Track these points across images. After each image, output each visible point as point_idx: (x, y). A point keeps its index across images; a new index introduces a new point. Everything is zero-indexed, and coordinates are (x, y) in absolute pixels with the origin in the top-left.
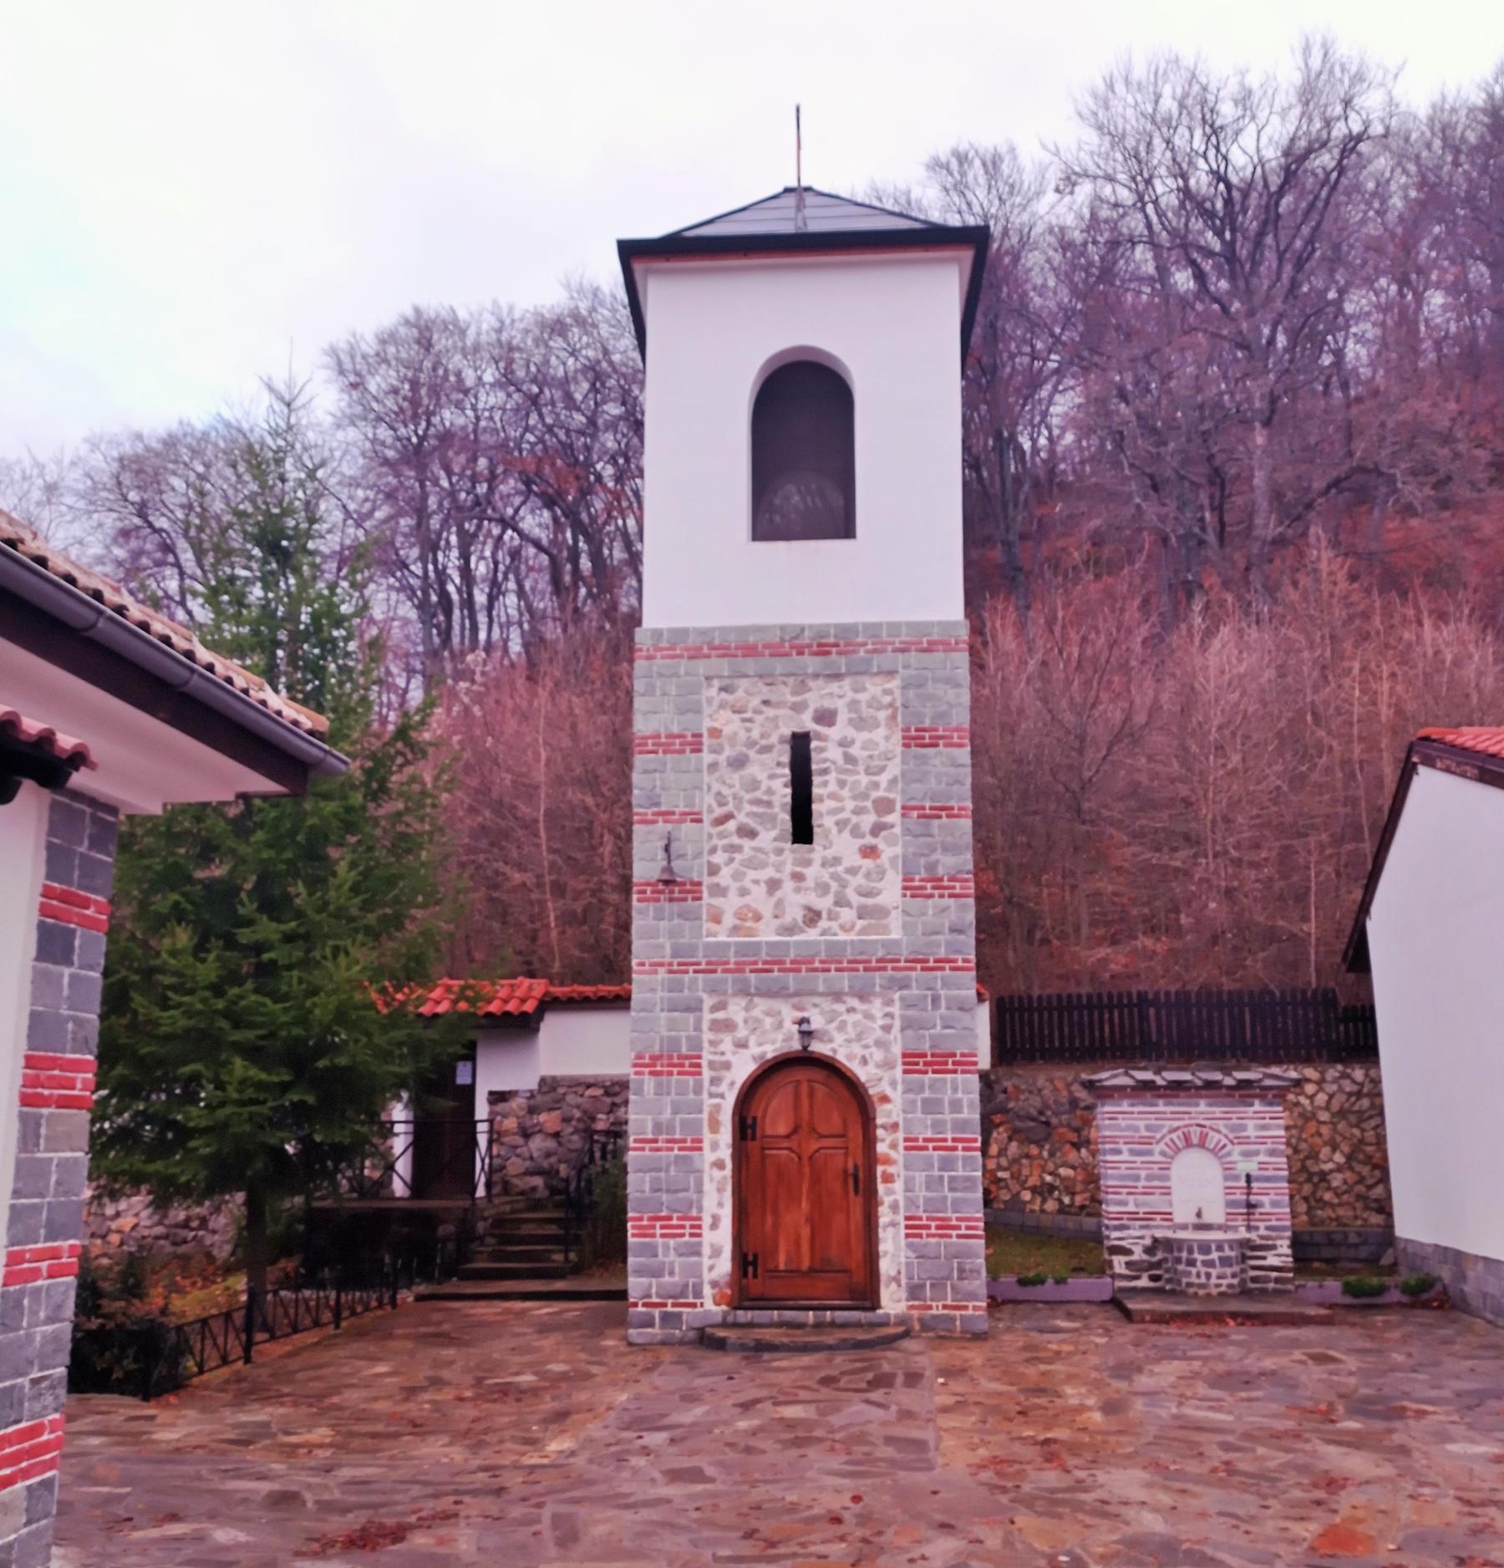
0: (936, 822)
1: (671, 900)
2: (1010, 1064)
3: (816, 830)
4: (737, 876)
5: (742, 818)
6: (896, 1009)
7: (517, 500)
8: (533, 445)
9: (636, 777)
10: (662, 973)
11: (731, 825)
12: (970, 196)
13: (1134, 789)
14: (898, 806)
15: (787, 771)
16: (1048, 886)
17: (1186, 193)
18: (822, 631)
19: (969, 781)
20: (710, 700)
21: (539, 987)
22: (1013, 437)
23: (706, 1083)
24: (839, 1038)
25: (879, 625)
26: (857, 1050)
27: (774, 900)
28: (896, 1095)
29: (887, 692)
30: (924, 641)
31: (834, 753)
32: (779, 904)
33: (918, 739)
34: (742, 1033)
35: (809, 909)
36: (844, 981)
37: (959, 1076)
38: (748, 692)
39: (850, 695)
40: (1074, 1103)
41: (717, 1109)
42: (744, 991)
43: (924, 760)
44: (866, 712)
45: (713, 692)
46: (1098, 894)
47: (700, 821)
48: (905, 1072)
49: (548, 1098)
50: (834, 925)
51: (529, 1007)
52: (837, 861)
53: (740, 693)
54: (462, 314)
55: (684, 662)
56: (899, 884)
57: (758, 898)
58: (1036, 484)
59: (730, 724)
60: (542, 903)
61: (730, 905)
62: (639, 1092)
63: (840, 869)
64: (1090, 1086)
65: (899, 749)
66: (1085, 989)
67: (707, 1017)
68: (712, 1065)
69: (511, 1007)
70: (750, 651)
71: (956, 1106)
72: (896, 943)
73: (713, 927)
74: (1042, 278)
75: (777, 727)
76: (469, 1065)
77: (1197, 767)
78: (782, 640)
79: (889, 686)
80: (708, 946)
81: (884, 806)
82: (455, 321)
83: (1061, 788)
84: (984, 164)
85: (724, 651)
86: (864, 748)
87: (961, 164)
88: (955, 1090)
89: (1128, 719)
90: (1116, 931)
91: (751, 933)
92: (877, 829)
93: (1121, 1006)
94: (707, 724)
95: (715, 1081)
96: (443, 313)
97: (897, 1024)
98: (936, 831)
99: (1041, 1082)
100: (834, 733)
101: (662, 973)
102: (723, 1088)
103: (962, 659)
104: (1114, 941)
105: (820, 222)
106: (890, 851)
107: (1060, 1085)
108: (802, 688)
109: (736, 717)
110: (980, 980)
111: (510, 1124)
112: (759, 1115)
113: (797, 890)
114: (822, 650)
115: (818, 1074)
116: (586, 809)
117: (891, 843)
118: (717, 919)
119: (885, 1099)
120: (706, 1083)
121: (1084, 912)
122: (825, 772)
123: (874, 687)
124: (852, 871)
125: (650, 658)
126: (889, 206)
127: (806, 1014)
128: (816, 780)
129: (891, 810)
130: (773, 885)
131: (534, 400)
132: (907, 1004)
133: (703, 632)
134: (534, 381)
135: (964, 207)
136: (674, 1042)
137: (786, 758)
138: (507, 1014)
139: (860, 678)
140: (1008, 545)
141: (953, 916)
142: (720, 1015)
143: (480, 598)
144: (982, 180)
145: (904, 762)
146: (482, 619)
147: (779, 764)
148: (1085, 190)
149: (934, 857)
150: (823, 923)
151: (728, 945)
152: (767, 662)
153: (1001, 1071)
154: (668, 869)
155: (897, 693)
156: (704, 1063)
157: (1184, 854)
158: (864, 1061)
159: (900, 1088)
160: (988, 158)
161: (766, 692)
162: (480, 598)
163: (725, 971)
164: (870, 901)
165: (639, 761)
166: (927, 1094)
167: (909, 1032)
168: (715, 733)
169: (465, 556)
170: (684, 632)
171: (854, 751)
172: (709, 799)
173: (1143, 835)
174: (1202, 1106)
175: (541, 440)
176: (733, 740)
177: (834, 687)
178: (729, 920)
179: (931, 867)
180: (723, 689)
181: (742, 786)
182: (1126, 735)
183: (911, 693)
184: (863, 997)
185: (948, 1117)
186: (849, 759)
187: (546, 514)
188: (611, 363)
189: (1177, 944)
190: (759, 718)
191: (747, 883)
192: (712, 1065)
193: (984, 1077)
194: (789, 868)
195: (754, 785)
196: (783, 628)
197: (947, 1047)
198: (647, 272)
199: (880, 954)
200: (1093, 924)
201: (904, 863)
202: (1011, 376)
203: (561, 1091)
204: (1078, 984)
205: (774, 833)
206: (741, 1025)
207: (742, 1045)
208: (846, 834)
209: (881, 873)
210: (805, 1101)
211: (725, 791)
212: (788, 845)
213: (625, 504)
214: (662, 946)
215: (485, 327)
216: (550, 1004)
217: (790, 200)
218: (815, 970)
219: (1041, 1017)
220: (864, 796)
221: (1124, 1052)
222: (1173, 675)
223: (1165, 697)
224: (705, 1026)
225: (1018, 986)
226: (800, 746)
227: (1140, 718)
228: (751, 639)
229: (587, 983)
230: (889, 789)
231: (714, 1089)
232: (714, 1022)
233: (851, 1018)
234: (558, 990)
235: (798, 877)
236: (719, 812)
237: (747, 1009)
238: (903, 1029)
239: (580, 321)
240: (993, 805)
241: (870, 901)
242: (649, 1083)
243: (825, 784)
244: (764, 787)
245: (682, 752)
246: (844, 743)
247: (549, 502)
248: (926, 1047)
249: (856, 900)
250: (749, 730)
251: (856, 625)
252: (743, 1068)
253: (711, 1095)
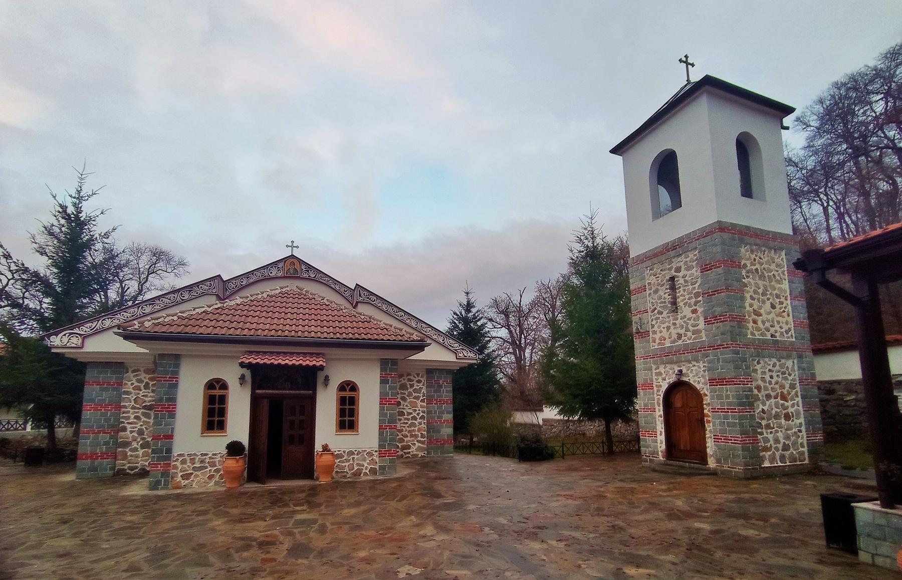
18: (673, 242)
24: (691, 375)
31: (681, 281)
36: (690, 356)
52: (685, 316)
57: (665, 334)
67: (654, 371)
81: (697, 295)
95: (658, 391)
108: (671, 262)
124: (689, 319)
130: (668, 328)
161: (662, 267)
178: (657, 341)
184: (697, 361)
186: (686, 281)
197: (723, 376)
209: (698, 318)
220: (691, 293)
235: (674, 324)
252: (665, 386)
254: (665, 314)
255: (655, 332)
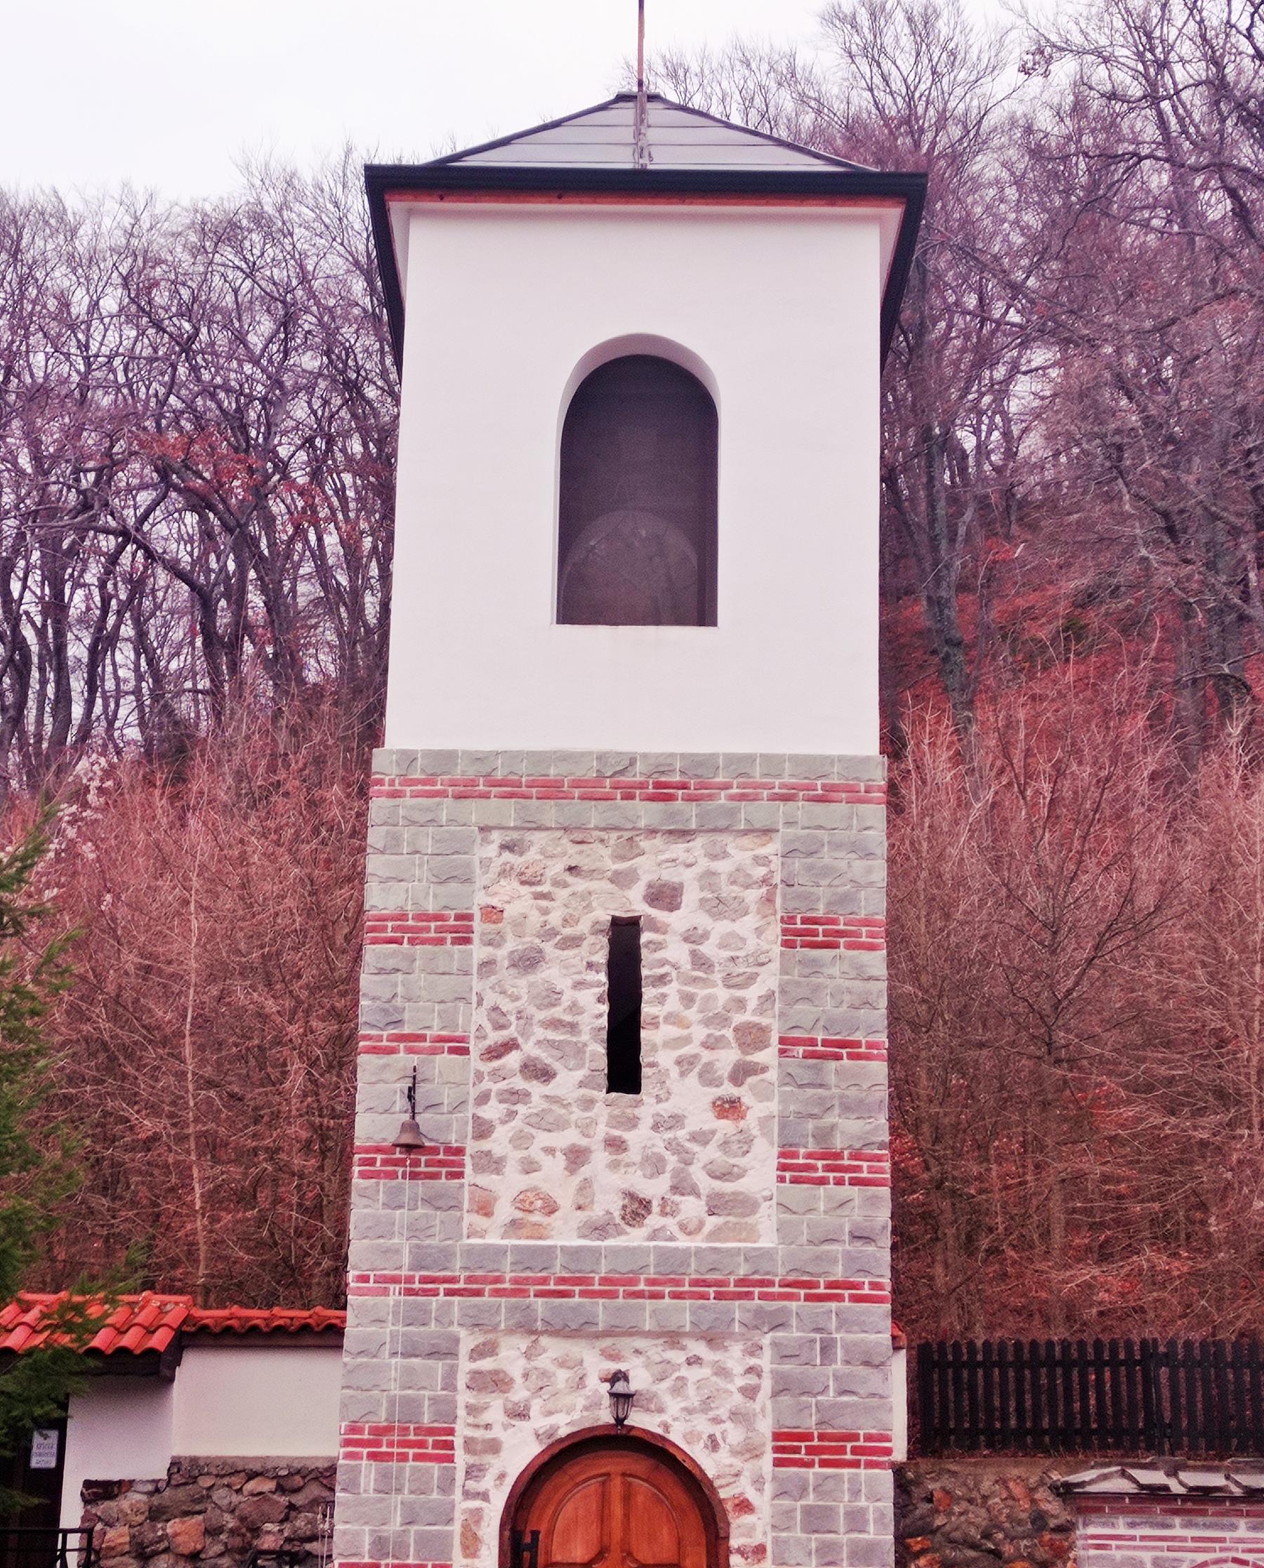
0: (833, 1065)
1: (414, 1176)
2: (937, 1453)
3: (645, 1071)
4: (520, 1140)
5: (529, 1048)
6: (765, 1361)
7: (145, 498)
8: (178, 415)
9: (366, 980)
10: (395, 1296)
11: (513, 1060)
12: (887, 65)
13: (1137, 1010)
14: (774, 1039)
15: (603, 977)
16: (999, 1159)
17: (1218, 87)
18: (662, 764)
19: (883, 1002)
20: (485, 863)
21: (176, 1308)
22: (948, 434)
23: (460, 1475)
24: (673, 1406)
25: (750, 758)
26: (702, 1425)
27: (576, 1180)
28: (762, 1501)
29: (760, 861)
30: (822, 788)
31: (677, 952)
32: (586, 1185)
33: (806, 933)
34: (519, 1393)
35: (631, 1196)
36: (683, 1313)
37: (862, 1472)
38: (547, 852)
39: (704, 864)
40: (1039, 1519)
41: (477, 1515)
42: (527, 1328)
43: (815, 968)
44: (727, 890)
45: (492, 850)
46: (1079, 1177)
47: (465, 1051)
48: (778, 1463)
49: (181, 1494)
50: (671, 1223)
51: (160, 1340)
52: (677, 1120)
53: (532, 855)
54: (73, 204)
55: (448, 801)
56: (774, 1162)
57: (551, 1176)
58: (983, 504)
59: (517, 901)
60: (184, 1171)
61: (507, 1186)
62: (352, 1487)
63: (682, 1134)
64: (1066, 1492)
65: (777, 949)
66: (1058, 1334)
67: (465, 1366)
68: (469, 1444)
69: (127, 1340)
70: (551, 790)
71: (856, 1520)
72: (767, 1254)
73: (480, 1221)
74: (996, 201)
75: (588, 908)
76: (54, 1435)
77: (1235, 982)
78: (601, 777)
79: (762, 851)
80: (470, 1252)
81: (752, 1037)
82: (61, 215)
83: (1021, 1008)
84: (910, 20)
85: (511, 789)
86: (723, 946)
87: (873, 15)
88: (855, 1493)
89: (1128, 899)
90: (1108, 1239)
91: (539, 1231)
92: (741, 1073)
93: (1114, 1364)
94: (481, 899)
95: (473, 1472)
96: (42, 200)
97: (767, 1384)
98: (832, 1079)
99: (986, 1485)
100: (677, 920)
101: (395, 1296)
102: (487, 1483)
103: (876, 814)
104: (1104, 1255)
105: (675, 151)
106: (761, 1107)
107: (1017, 1490)
108: (629, 849)
109: (526, 890)
110: (896, 1316)
111: (118, 1536)
112: (543, 1528)
113: (614, 1165)
114: (662, 793)
115: (638, 1464)
116: (263, 1016)
117: (764, 1097)
118: (485, 1209)
119: (744, 1506)
120: (460, 1475)
121: (1056, 1206)
122: (662, 980)
123: (740, 853)
124: (701, 1138)
125: (394, 795)
126: (783, 134)
127: (622, 1366)
128: (648, 993)
129: (761, 1044)
130: (576, 1157)
131: (186, 345)
132: (783, 1354)
133: (478, 758)
134: (186, 312)
135: (878, 80)
136: (412, 1405)
137: (601, 957)
138: (123, 1351)
139: (719, 837)
140: (937, 604)
141: (856, 1215)
142: (486, 1364)
143: (77, 650)
144: (907, 42)
145: (784, 971)
146: (77, 684)
147: (590, 966)
148: (1065, 70)
149: (829, 1119)
150: (654, 1220)
151: (502, 1251)
152: (576, 809)
153: (924, 1465)
154: (412, 1127)
155: (776, 863)
156: (458, 1441)
157: (1212, 1120)
158: (713, 1444)
159: (769, 1488)
160: (917, 11)
161: (574, 855)
162: (77, 650)
163: (497, 1293)
164: (728, 1187)
165: (372, 954)
166: (811, 1500)
167: (785, 1399)
168: (493, 914)
169: (54, 580)
170: (449, 757)
171: (708, 949)
172: (480, 1017)
173: (1150, 1088)
174: (1242, 1529)
175: (190, 406)
176: (519, 924)
177: (678, 850)
178: (504, 1211)
179: (824, 1135)
180: (507, 847)
181: (533, 998)
182: (1127, 925)
183: (797, 864)
184: (713, 1339)
185: (843, 1538)
186: (700, 962)
187: (191, 519)
188: (312, 294)
189: (1205, 1265)
190: (562, 894)
191: (535, 1152)
192: (469, 1444)
193: (899, 1470)
194: (601, 1131)
195: (551, 997)
196: (601, 757)
197: (843, 1424)
198: (410, 213)
199: (742, 1271)
200: (1072, 1227)
201: (783, 1127)
202: (946, 338)
203: (205, 1482)
204: (1047, 1321)
205: (580, 1074)
206: (519, 1380)
207: (519, 1413)
208: (693, 1078)
209: (747, 1143)
210: (617, 1509)
211: (506, 1005)
212: (601, 1095)
213: (323, 513)
214: (397, 1251)
215: (107, 223)
216: (194, 1337)
217: (626, 113)
218: (639, 1295)
219: (988, 1377)
220: (721, 1020)
221: (1123, 1437)
222: (1197, 833)
223: (1185, 869)
224: (462, 1380)
225: (951, 1322)
226: (624, 940)
227: (1146, 898)
228: (552, 772)
229: (252, 1303)
230: (760, 1010)
231: (471, 1485)
232: (476, 1375)
233: (693, 1374)
234: (211, 1315)
235: (615, 1145)
236: (495, 1037)
237: (528, 1355)
238: (775, 1394)
239: (258, 218)
240: (915, 1027)
241: (728, 1187)
242: (368, 1472)
243: (662, 999)
244: (566, 1000)
245: (441, 942)
246: (693, 937)
247: (199, 502)
248: (810, 1423)
249: (706, 1184)
250: (545, 912)
251: (714, 756)
252: (520, 1451)
253: (467, 1494)
254: (568, 1081)
255: (492, 1164)
